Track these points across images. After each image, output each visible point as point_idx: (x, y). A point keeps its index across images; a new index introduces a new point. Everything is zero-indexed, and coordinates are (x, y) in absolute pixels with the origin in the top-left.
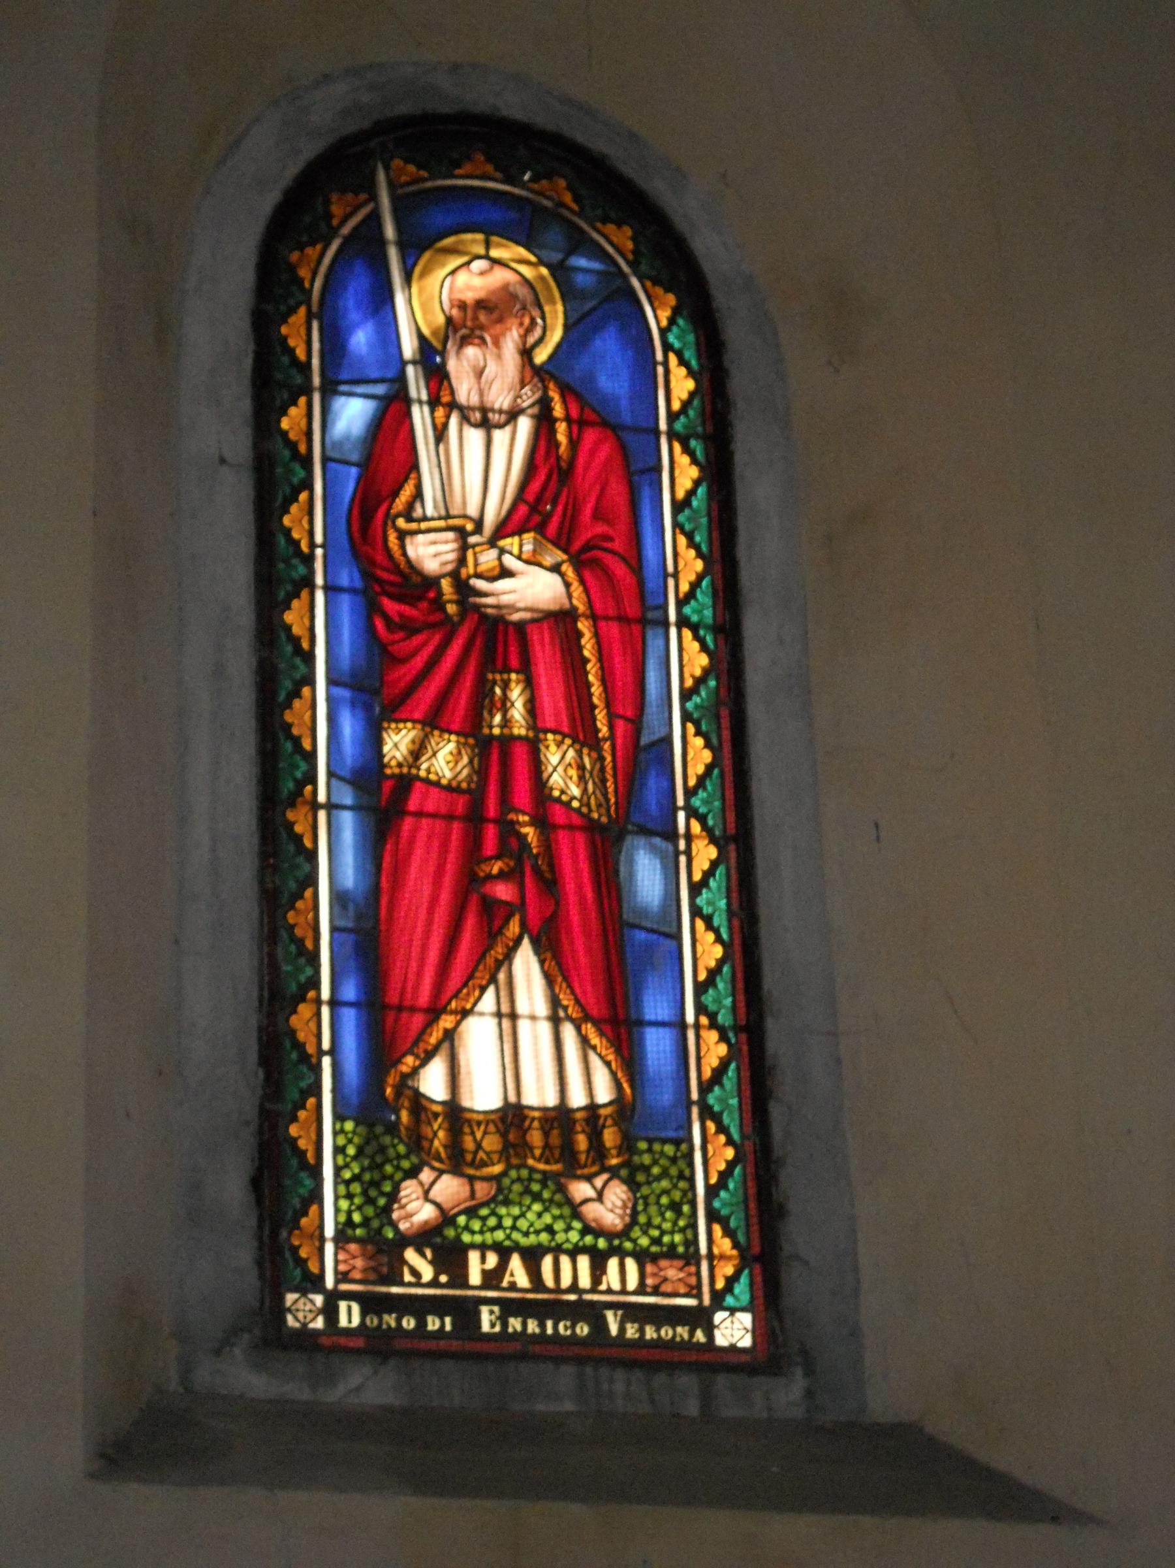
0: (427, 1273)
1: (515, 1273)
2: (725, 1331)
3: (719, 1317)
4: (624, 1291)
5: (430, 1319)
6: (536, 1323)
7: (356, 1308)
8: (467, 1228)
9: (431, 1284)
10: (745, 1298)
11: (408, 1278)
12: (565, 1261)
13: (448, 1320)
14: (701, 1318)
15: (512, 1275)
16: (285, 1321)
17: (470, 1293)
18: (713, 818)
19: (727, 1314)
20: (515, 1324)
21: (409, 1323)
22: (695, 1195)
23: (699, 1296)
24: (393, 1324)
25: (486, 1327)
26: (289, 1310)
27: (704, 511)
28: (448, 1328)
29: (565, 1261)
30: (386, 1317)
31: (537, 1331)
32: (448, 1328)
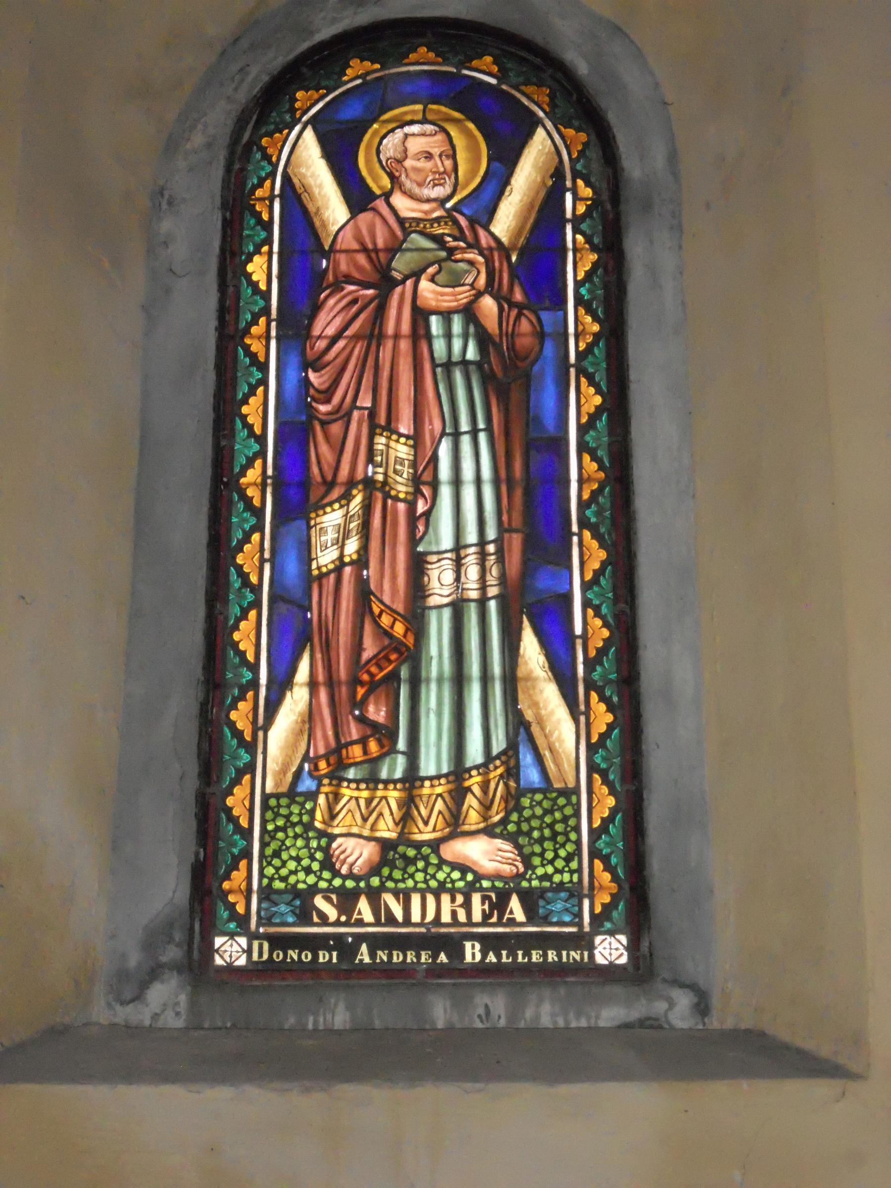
0: (332, 913)
1: (515, 911)
2: (603, 951)
3: (598, 939)
4: (470, 923)
5: (321, 953)
6: (414, 953)
7: (478, 946)
8: (390, 878)
9: (338, 923)
10: (621, 924)
11: (316, 919)
12: (430, 899)
13: (335, 954)
14: (583, 941)
15: (360, 913)
16: (213, 959)
17: (517, 929)
18: (607, 607)
19: (245, 947)
20: (382, 955)
21: (307, 956)
22: (260, 862)
23: (580, 925)
24: (296, 957)
25: (468, 958)
26: (217, 951)
27: (234, 528)
28: (335, 960)
29: (431, 899)
30: (290, 952)
31: (556, 959)
32: (335, 960)
